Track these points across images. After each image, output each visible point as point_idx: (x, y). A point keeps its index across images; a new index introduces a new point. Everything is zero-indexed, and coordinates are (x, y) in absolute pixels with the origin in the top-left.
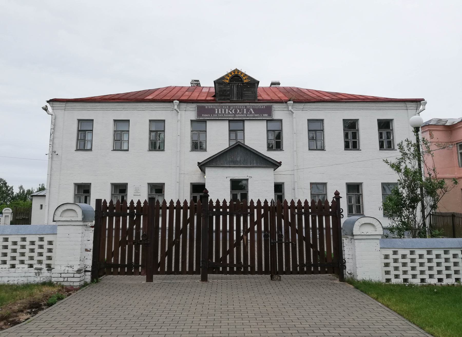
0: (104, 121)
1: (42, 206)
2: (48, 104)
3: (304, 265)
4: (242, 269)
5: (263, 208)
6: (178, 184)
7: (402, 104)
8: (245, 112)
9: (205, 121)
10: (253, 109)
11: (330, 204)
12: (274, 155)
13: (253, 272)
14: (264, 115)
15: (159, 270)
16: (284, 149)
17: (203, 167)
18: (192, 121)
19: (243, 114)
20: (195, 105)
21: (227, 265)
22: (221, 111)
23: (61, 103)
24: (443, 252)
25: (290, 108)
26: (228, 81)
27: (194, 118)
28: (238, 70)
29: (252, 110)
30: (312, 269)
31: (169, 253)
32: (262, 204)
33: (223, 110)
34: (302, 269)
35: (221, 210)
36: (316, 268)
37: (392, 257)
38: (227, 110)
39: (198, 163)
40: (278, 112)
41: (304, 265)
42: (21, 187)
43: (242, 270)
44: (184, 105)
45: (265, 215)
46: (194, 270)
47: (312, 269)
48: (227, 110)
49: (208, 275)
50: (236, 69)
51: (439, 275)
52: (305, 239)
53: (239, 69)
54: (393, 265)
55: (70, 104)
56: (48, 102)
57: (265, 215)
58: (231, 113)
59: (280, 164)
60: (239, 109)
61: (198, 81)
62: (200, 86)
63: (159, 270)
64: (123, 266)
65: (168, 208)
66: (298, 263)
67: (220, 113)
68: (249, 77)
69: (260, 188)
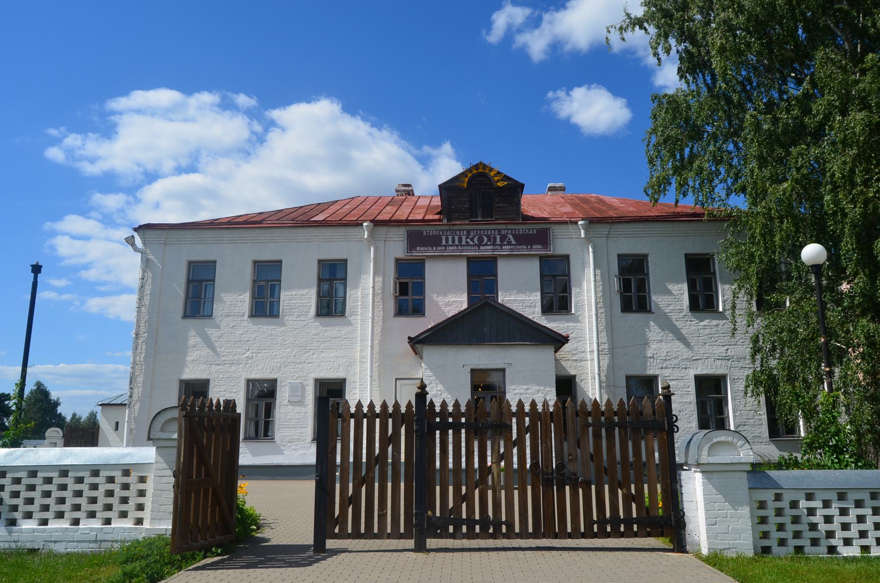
0: (300, 258)
2: (135, 234)
3: (607, 522)
4: (491, 528)
5: (390, 416)
7: (639, 227)
8: (498, 242)
10: (514, 236)
12: (556, 324)
13: (510, 534)
14: (534, 247)
15: (337, 531)
17: (418, 346)
20: (402, 232)
21: (463, 522)
23: (159, 232)
24: (869, 496)
28: (485, 165)
29: (511, 237)
30: (622, 529)
31: (354, 500)
32: (527, 408)
33: (456, 238)
34: (602, 529)
35: (463, 420)
36: (629, 527)
37: (772, 505)
39: (409, 338)
40: (565, 242)
41: (607, 522)
43: (491, 531)
44: (383, 230)
45: (532, 429)
46: (402, 530)
47: (622, 529)
48: (464, 238)
49: (428, 540)
50: (481, 163)
51: (862, 540)
53: (487, 163)
54: (774, 520)
55: (175, 233)
56: (135, 230)
57: (532, 429)
58: (471, 243)
60: (487, 236)
61: (409, 185)
62: (413, 195)
63: (337, 531)
64: (484, 522)
65: (378, 416)
66: (595, 518)
67: (450, 243)
68: (505, 176)
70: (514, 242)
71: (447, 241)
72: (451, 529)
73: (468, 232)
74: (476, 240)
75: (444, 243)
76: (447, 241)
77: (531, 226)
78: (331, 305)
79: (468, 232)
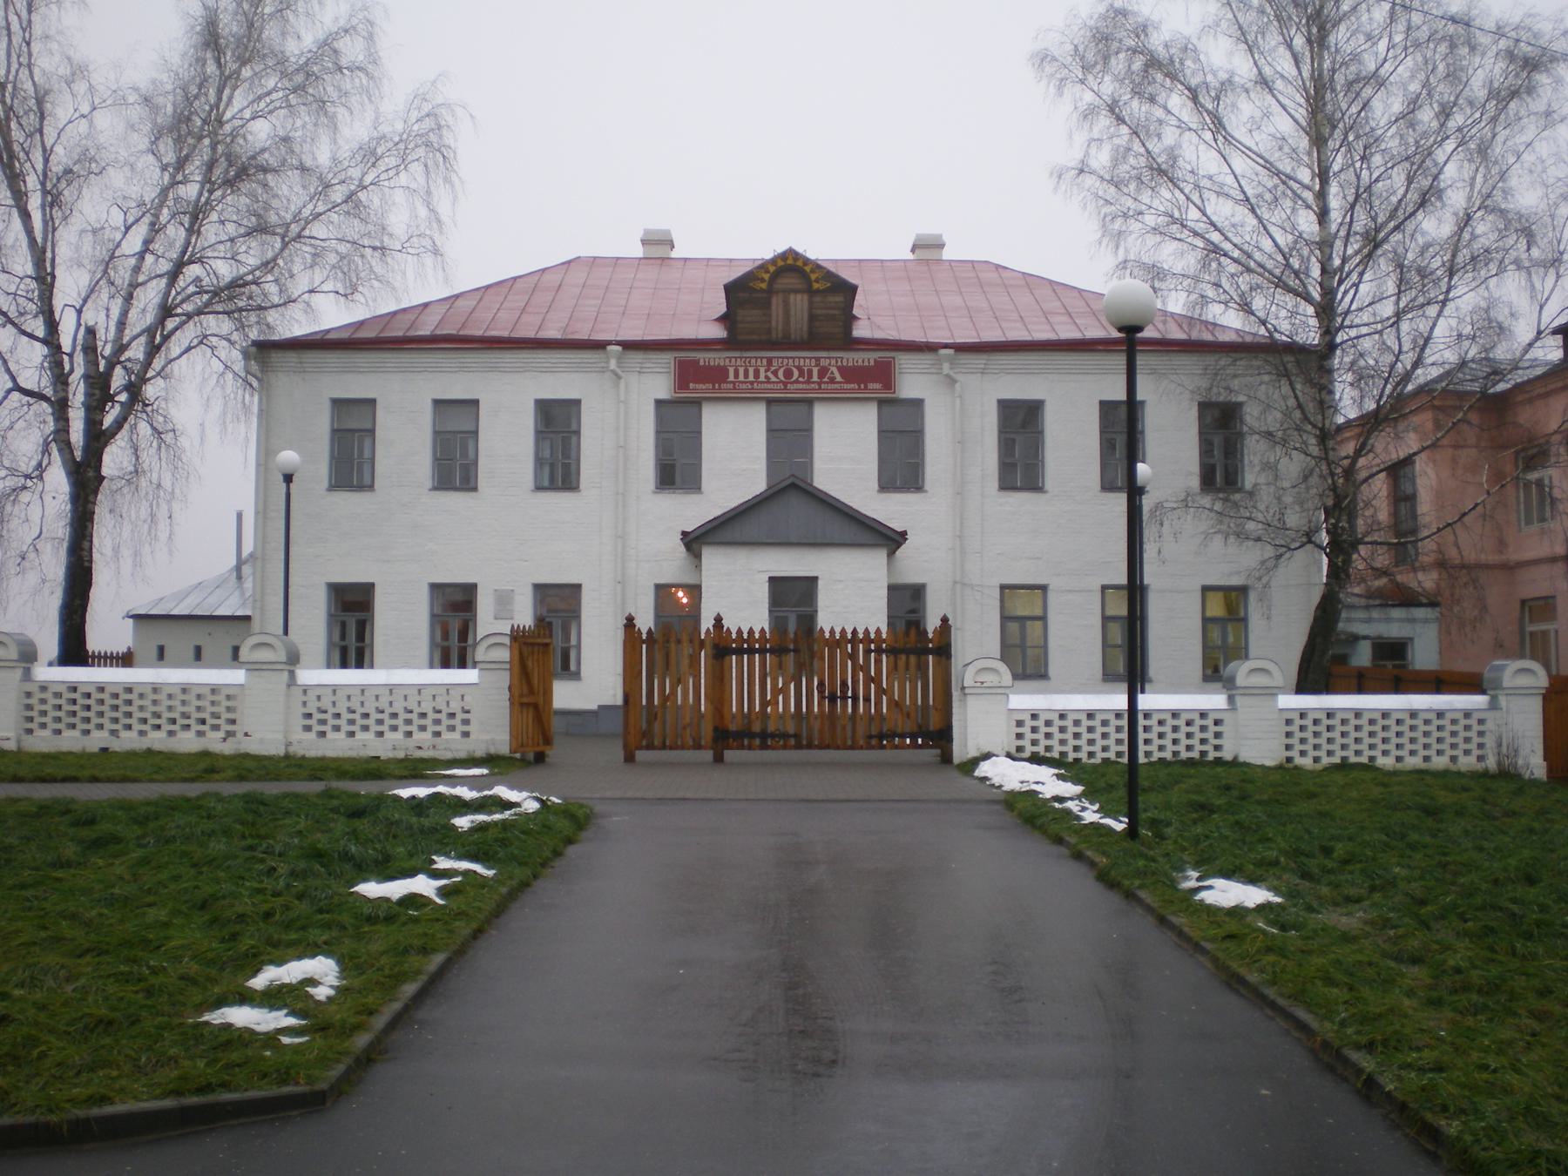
0: (405, 403)
1: (161, 650)
6: (619, 587)
8: (815, 378)
9: (697, 403)
10: (840, 369)
11: (930, 635)
12: (888, 509)
14: (871, 386)
16: (927, 487)
17: (695, 546)
18: (659, 403)
19: (808, 382)
20: (668, 358)
22: (746, 375)
25: (946, 367)
26: (764, 286)
27: (664, 394)
29: (835, 370)
38: (762, 370)
39: (684, 534)
40: (913, 381)
42: (718, 620)
44: (636, 358)
48: (762, 370)
50: (790, 266)
52: (884, 692)
53: (800, 249)
55: (311, 357)
58: (773, 379)
59: (903, 535)
60: (799, 368)
67: (741, 378)
69: (852, 596)
70: (839, 378)
71: (736, 375)
72: (746, 742)
73: (770, 361)
74: (781, 374)
75: (731, 378)
76: (736, 375)
77: (866, 355)
78: (558, 466)
79: (770, 361)
